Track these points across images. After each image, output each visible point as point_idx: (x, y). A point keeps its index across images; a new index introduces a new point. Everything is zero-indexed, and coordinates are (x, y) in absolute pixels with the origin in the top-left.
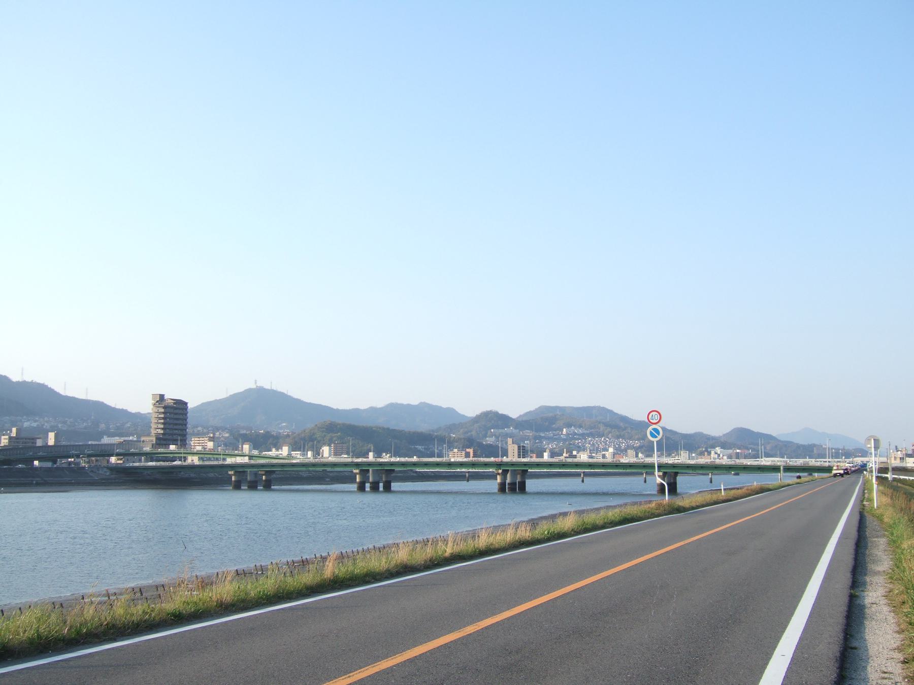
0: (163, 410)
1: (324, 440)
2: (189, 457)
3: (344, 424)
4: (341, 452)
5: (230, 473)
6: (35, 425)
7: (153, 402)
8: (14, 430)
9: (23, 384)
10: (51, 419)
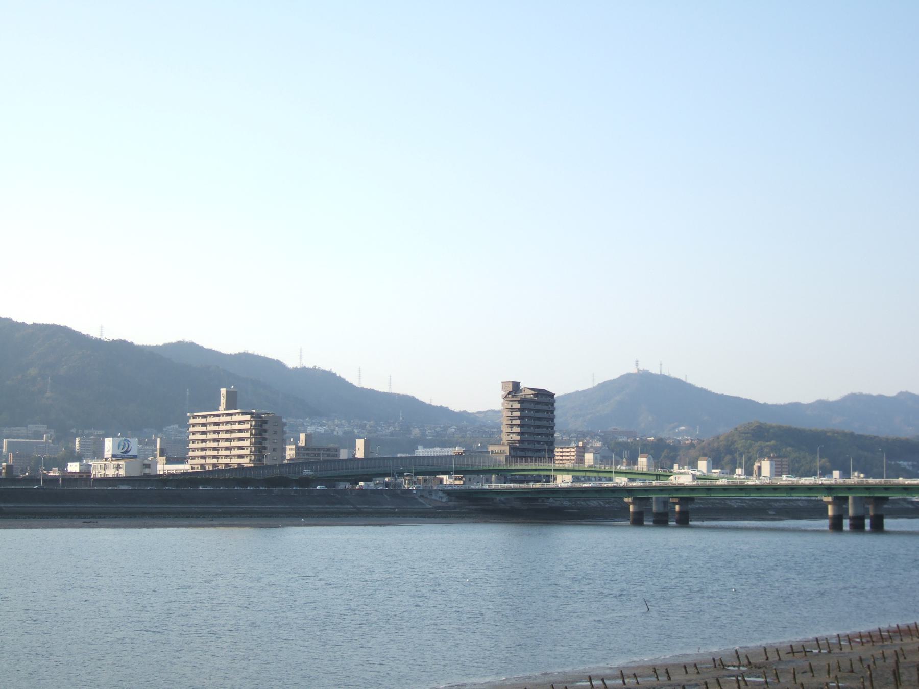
0: (518, 406)
1: (749, 452)
2: (558, 476)
3: (779, 427)
4: (780, 470)
5: (626, 500)
6: (321, 430)
7: (504, 393)
8: (302, 436)
9: (303, 372)
10: (343, 421)
